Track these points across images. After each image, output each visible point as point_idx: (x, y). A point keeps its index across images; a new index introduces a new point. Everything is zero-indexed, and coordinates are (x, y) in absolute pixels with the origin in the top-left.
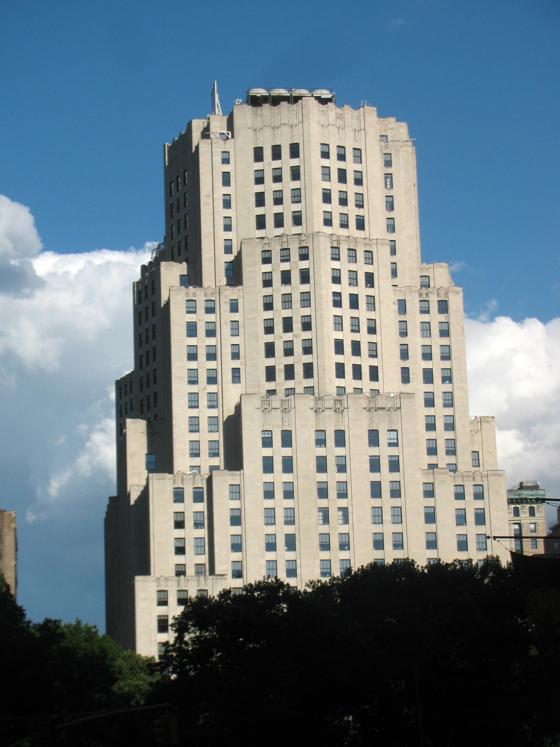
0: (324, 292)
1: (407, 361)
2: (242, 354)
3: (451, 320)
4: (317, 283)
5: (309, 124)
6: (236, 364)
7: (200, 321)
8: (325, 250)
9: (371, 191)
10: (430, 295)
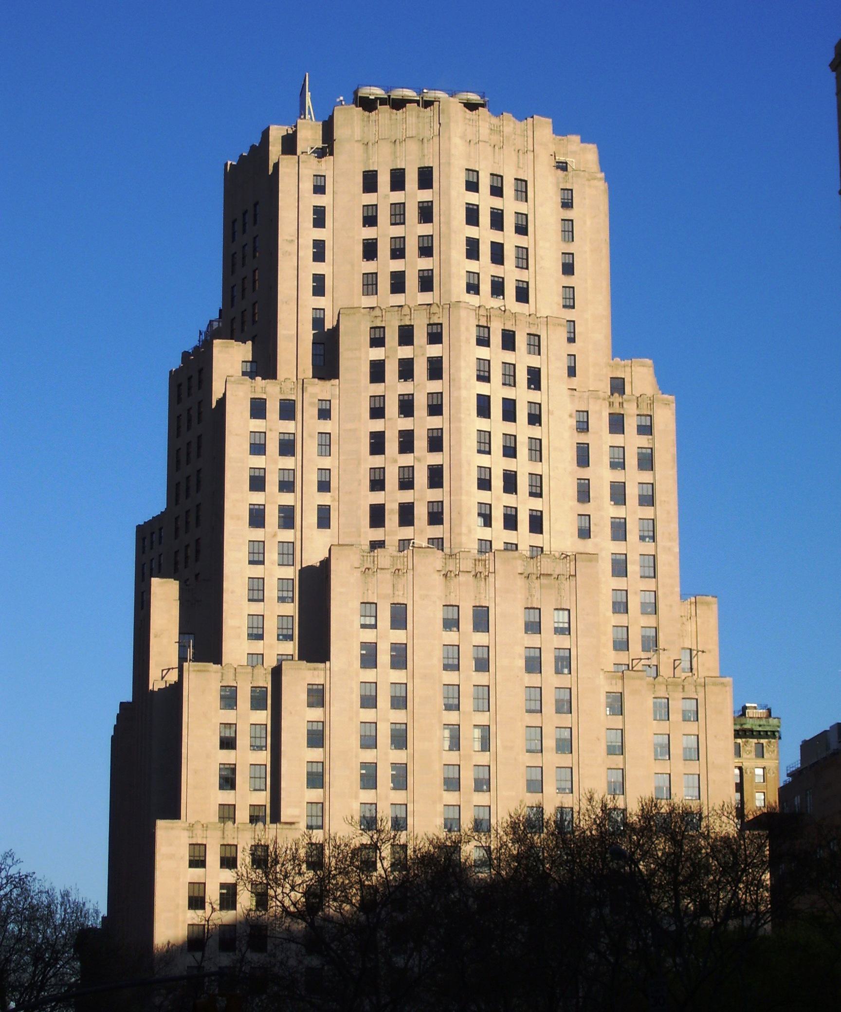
0: (464, 393)
1: (586, 505)
2: (334, 484)
3: (657, 446)
4: (454, 380)
5: (449, 138)
6: (325, 499)
7: (271, 430)
8: (467, 329)
9: (541, 244)
10: (625, 406)
